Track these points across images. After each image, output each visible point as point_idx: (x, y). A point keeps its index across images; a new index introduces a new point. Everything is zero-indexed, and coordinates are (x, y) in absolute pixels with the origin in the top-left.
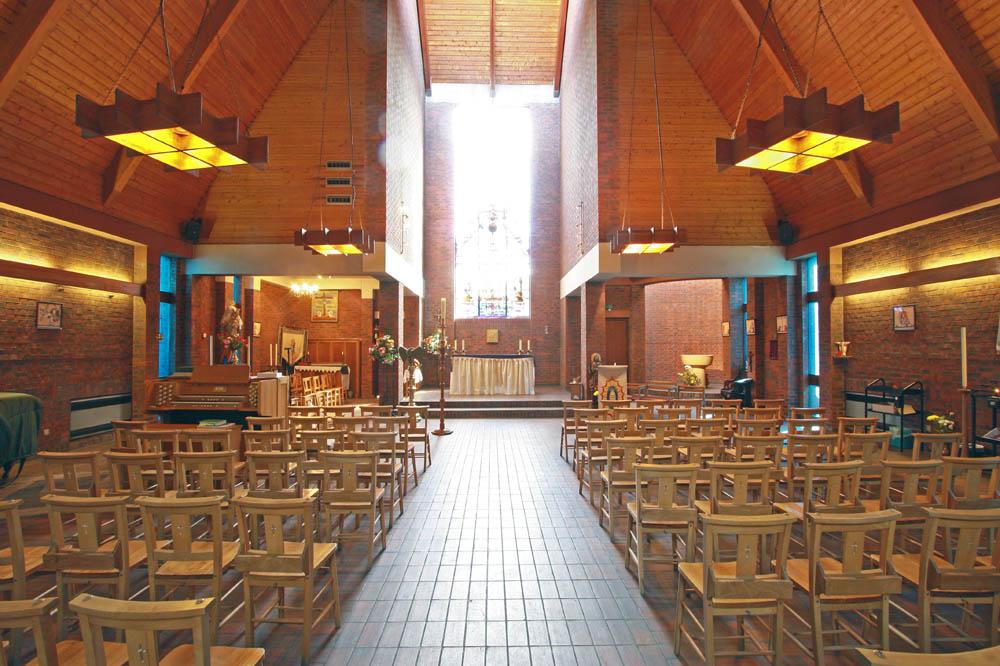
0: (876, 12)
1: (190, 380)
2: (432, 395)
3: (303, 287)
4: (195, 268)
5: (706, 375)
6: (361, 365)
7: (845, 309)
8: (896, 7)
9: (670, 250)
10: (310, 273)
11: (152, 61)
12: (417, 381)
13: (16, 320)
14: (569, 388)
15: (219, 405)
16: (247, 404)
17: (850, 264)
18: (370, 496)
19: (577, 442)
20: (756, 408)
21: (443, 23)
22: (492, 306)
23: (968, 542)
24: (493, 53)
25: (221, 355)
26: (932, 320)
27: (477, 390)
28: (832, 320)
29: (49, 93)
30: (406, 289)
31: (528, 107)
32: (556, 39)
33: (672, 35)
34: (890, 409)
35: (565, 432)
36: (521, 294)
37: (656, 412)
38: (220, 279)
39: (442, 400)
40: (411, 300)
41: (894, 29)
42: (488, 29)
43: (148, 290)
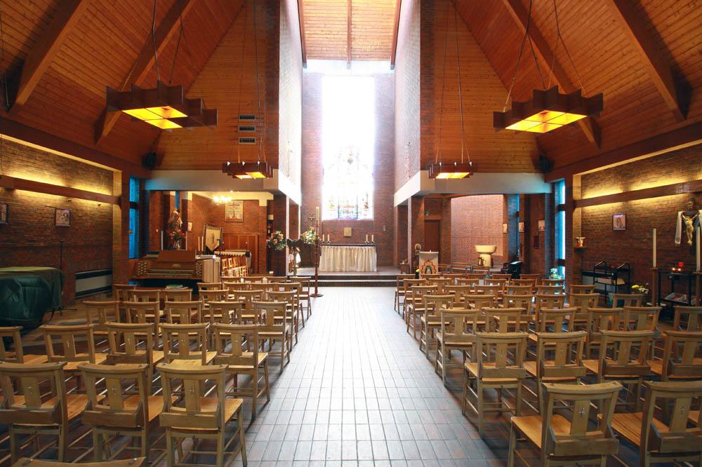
0: (601, 24)
1: (148, 258)
2: (309, 272)
3: (221, 198)
4: (153, 185)
5: (492, 259)
6: (258, 251)
7: (582, 216)
8: (614, 21)
9: (466, 177)
10: (226, 188)
11: (128, 51)
12: (297, 262)
13: (43, 220)
14: (399, 267)
15: (176, 276)
16: (195, 275)
17: (586, 186)
18: (282, 329)
19: (405, 300)
20: (521, 279)
21: (315, 19)
22: (347, 212)
23: (624, 350)
24: (350, 39)
25: (168, 244)
26: (636, 224)
27: (338, 268)
28: (574, 223)
29: (64, 73)
30: (290, 200)
31: (373, 76)
32: (392, 30)
33: (470, 31)
34: (608, 281)
35: (398, 294)
36: (367, 203)
37: (456, 282)
38: (166, 193)
39: (316, 274)
40: (294, 207)
41: (613, 35)
42: (346, 23)
43: (122, 201)
